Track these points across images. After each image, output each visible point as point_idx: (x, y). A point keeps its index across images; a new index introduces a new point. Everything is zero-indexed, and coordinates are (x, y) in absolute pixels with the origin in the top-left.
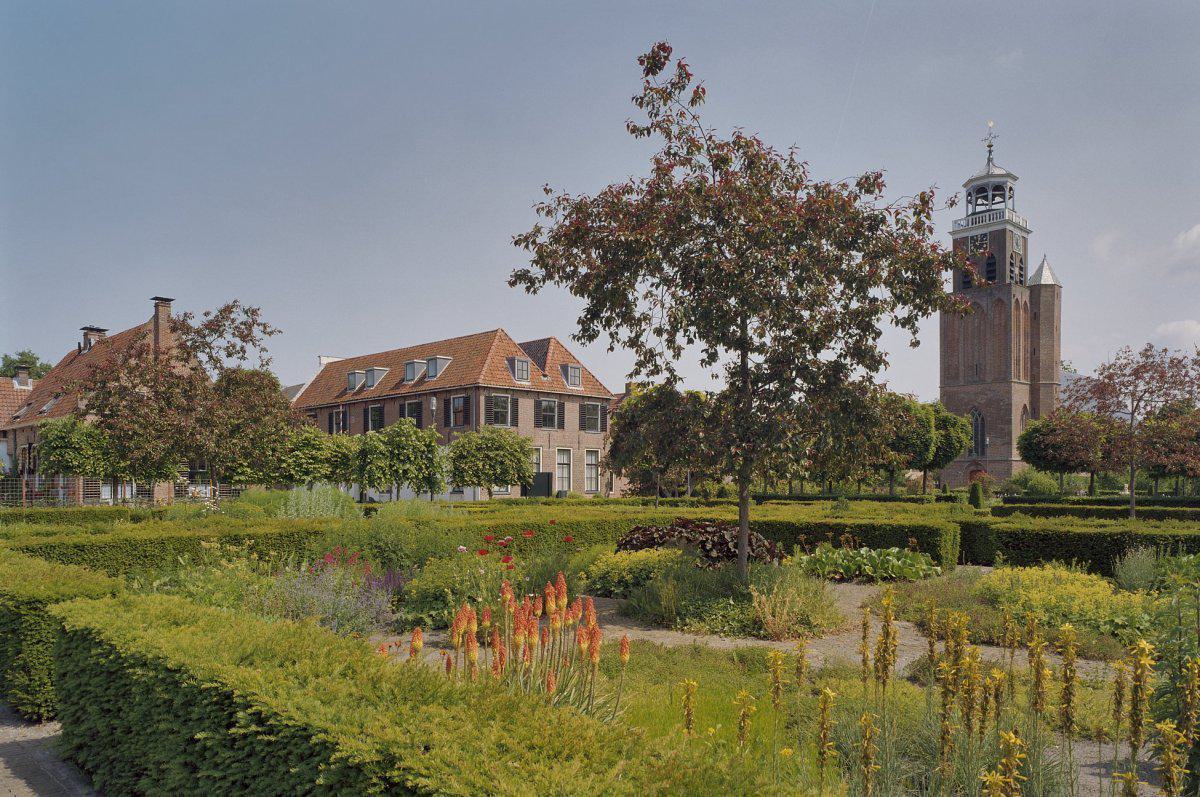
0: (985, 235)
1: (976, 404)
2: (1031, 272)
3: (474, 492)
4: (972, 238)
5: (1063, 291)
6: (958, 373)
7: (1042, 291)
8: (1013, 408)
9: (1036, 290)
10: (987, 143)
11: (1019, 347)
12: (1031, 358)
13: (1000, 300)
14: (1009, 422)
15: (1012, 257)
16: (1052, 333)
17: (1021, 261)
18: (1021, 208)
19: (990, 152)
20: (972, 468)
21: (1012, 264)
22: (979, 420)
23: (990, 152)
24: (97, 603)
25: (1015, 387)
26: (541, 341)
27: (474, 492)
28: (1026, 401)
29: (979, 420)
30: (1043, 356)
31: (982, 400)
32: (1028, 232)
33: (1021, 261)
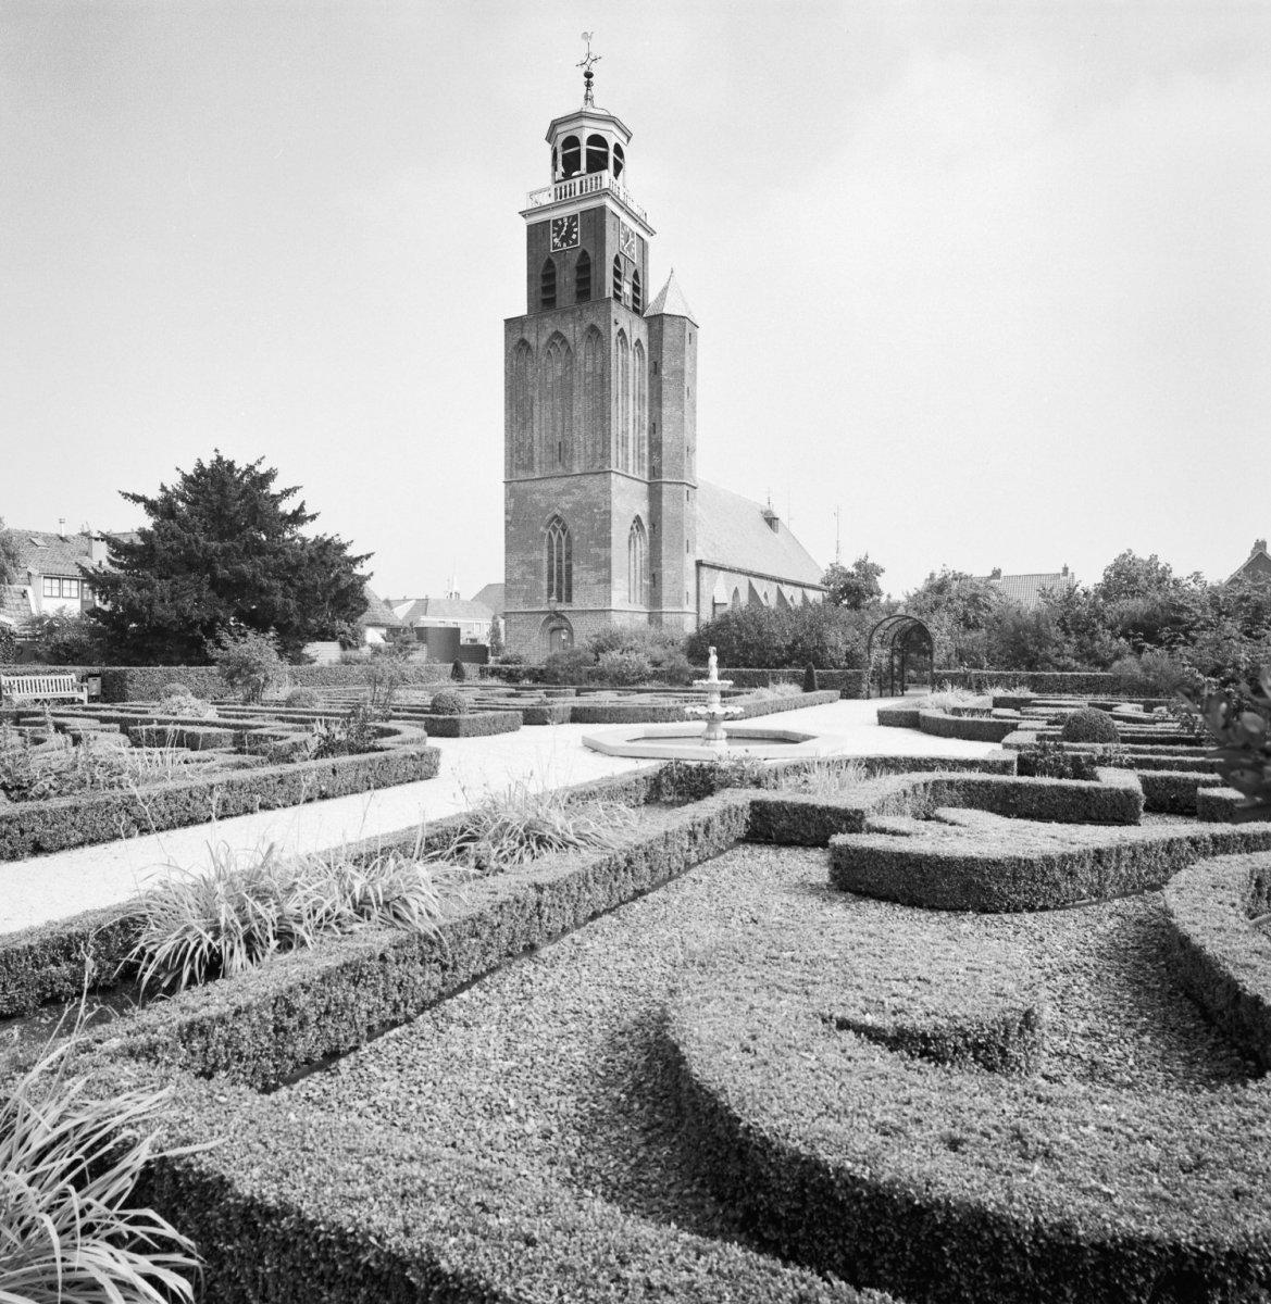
0: (574, 218)
1: (558, 512)
2: (652, 295)
3: (654, 598)
4: (555, 222)
5: (703, 337)
6: (532, 458)
7: (665, 325)
8: (615, 519)
9: (656, 323)
10: (585, 68)
11: (628, 416)
12: (650, 438)
13: (593, 328)
14: (607, 543)
15: (617, 260)
16: (681, 399)
17: (636, 275)
18: (637, 186)
19: (588, 85)
20: (553, 624)
21: (617, 274)
22: (564, 538)
23: (588, 85)
24: (8, 802)
25: (617, 482)
26: (507, 537)
27: (654, 598)
28: (642, 508)
29: (564, 538)
30: (667, 435)
31: (566, 503)
32: (651, 232)
33: (636, 275)
